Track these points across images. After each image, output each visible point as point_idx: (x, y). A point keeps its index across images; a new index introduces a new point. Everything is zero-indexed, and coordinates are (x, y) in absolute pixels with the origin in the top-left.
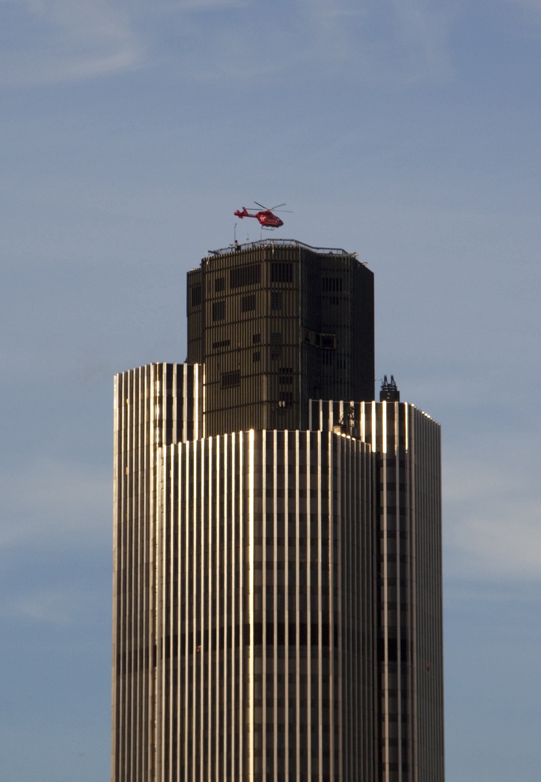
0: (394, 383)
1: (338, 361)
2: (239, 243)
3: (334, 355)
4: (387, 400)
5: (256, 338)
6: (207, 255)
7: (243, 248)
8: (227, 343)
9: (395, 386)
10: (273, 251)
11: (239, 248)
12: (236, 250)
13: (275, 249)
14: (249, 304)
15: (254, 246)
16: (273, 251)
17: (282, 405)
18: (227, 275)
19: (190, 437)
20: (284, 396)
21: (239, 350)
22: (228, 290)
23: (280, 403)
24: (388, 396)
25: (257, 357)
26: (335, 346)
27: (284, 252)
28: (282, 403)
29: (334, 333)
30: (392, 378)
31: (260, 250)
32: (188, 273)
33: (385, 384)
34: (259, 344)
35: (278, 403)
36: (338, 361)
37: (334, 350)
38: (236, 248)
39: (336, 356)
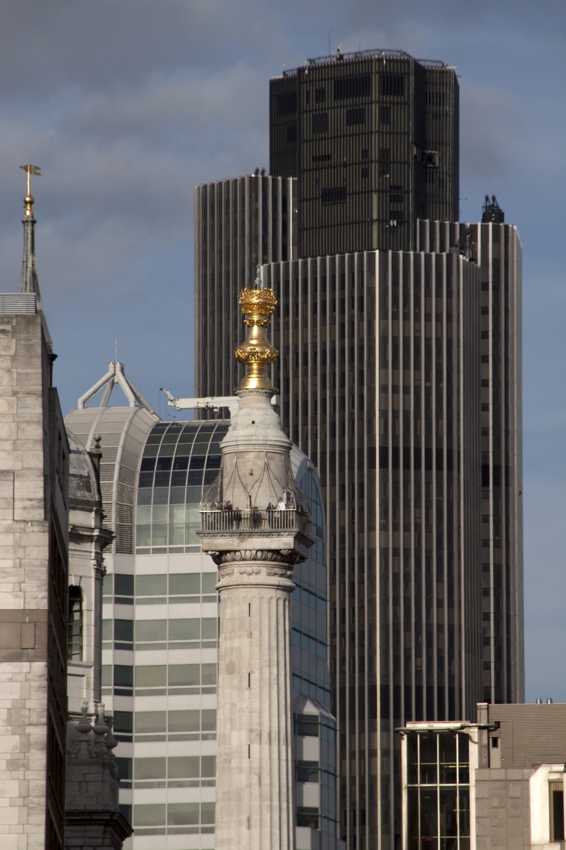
0: (497, 203)
1: (440, 179)
2: (341, 52)
3: (436, 173)
4: (493, 222)
5: (365, 153)
6: (306, 64)
7: (345, 57)
8: (328, 157)
9: (497, 207)
10: (385, 62)
11: (341, 57)
12: (338, 59)
13: (386, 59)
14: (356, 117)
15: (356, 57)
16: (385, 62)
17: (394, 225)
18: (329, 88)
19: (285, 257)
20: (394, 215)
21: (345, 165)
22: (330, 101)
23: (391, 222)
24: (492, 217)
25: (365, 173)
26: (437, 164)
27: (399, 64)
28: (393, 222)
29: (436, 150)
30: (494, 198)
31: (369, 61)
32: (274, 84)
33: (486, 204)
34: (367, 160)
35: (390, 222)
36: (440, 179)
37: (436, 168)
38: (338, 56)
39: (438, 174)
